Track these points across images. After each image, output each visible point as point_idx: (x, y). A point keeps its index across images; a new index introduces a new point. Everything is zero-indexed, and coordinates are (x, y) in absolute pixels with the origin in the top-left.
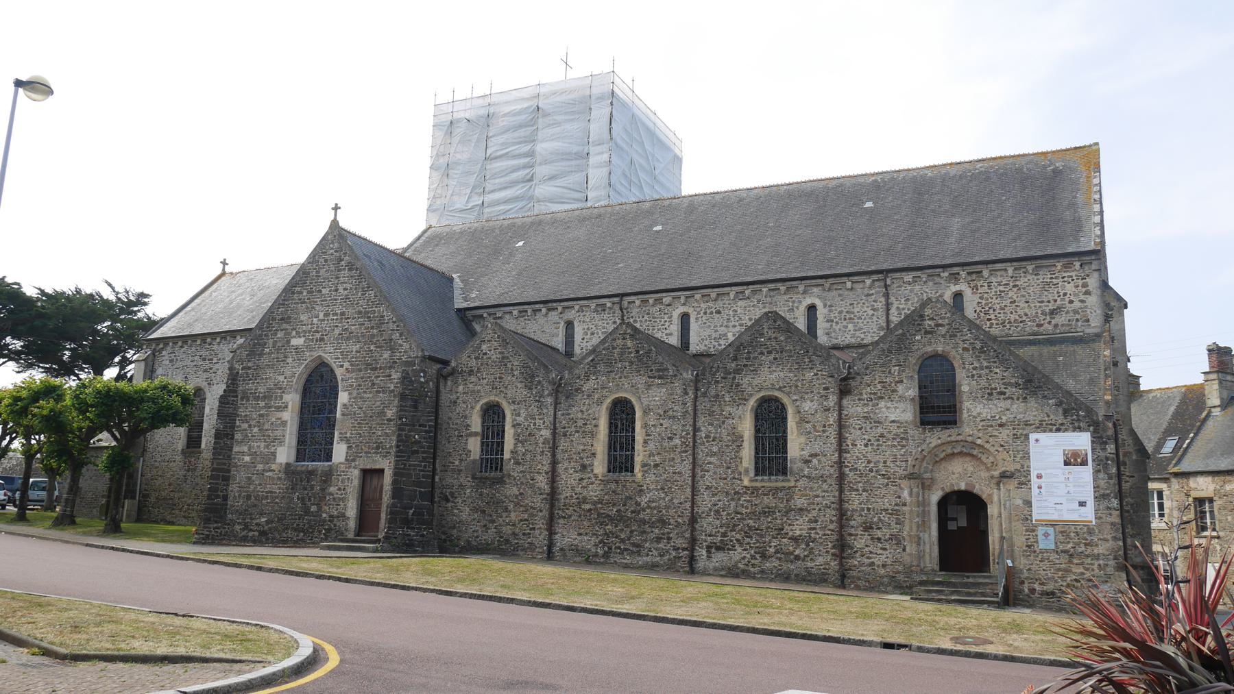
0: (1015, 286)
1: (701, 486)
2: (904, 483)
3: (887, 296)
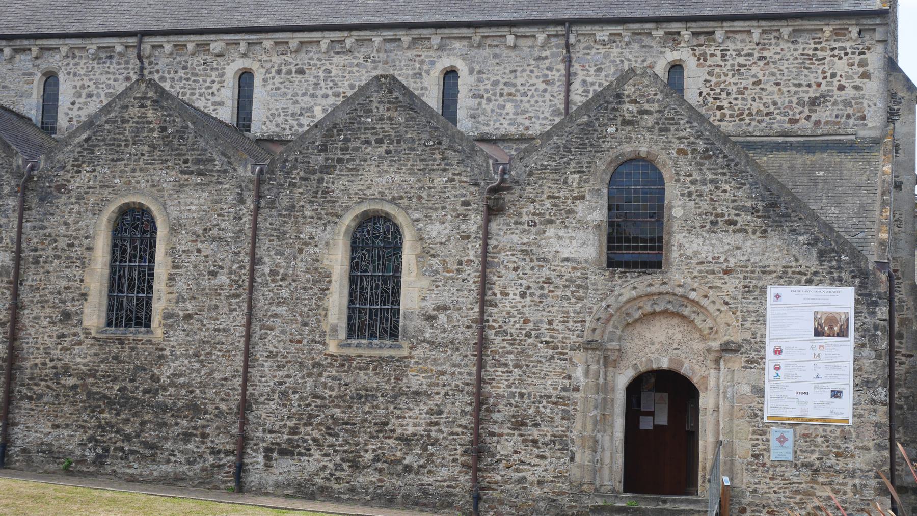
0: (761, 58)
1: (260, 352)
2: (579, 357)
3: (568, 61)
